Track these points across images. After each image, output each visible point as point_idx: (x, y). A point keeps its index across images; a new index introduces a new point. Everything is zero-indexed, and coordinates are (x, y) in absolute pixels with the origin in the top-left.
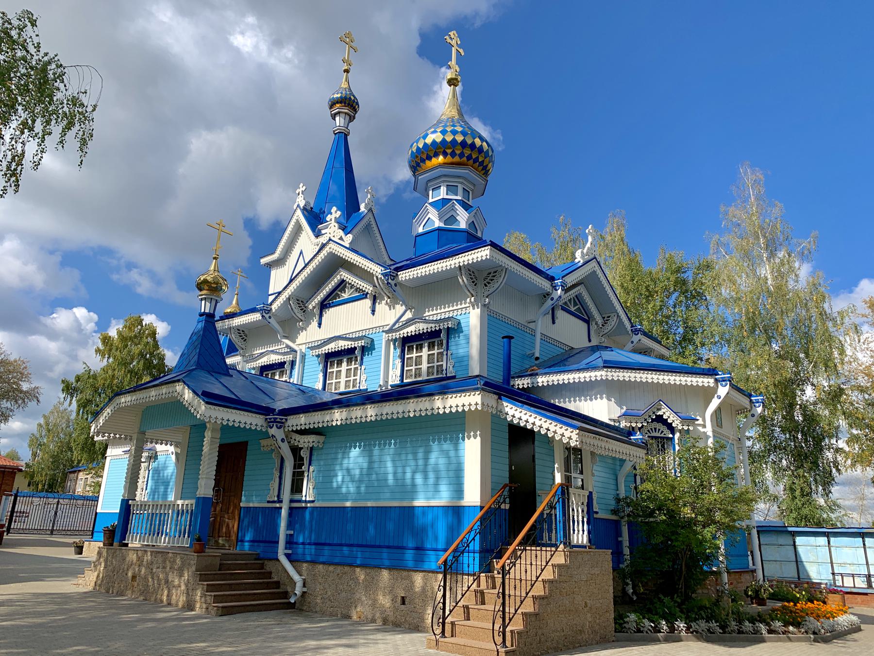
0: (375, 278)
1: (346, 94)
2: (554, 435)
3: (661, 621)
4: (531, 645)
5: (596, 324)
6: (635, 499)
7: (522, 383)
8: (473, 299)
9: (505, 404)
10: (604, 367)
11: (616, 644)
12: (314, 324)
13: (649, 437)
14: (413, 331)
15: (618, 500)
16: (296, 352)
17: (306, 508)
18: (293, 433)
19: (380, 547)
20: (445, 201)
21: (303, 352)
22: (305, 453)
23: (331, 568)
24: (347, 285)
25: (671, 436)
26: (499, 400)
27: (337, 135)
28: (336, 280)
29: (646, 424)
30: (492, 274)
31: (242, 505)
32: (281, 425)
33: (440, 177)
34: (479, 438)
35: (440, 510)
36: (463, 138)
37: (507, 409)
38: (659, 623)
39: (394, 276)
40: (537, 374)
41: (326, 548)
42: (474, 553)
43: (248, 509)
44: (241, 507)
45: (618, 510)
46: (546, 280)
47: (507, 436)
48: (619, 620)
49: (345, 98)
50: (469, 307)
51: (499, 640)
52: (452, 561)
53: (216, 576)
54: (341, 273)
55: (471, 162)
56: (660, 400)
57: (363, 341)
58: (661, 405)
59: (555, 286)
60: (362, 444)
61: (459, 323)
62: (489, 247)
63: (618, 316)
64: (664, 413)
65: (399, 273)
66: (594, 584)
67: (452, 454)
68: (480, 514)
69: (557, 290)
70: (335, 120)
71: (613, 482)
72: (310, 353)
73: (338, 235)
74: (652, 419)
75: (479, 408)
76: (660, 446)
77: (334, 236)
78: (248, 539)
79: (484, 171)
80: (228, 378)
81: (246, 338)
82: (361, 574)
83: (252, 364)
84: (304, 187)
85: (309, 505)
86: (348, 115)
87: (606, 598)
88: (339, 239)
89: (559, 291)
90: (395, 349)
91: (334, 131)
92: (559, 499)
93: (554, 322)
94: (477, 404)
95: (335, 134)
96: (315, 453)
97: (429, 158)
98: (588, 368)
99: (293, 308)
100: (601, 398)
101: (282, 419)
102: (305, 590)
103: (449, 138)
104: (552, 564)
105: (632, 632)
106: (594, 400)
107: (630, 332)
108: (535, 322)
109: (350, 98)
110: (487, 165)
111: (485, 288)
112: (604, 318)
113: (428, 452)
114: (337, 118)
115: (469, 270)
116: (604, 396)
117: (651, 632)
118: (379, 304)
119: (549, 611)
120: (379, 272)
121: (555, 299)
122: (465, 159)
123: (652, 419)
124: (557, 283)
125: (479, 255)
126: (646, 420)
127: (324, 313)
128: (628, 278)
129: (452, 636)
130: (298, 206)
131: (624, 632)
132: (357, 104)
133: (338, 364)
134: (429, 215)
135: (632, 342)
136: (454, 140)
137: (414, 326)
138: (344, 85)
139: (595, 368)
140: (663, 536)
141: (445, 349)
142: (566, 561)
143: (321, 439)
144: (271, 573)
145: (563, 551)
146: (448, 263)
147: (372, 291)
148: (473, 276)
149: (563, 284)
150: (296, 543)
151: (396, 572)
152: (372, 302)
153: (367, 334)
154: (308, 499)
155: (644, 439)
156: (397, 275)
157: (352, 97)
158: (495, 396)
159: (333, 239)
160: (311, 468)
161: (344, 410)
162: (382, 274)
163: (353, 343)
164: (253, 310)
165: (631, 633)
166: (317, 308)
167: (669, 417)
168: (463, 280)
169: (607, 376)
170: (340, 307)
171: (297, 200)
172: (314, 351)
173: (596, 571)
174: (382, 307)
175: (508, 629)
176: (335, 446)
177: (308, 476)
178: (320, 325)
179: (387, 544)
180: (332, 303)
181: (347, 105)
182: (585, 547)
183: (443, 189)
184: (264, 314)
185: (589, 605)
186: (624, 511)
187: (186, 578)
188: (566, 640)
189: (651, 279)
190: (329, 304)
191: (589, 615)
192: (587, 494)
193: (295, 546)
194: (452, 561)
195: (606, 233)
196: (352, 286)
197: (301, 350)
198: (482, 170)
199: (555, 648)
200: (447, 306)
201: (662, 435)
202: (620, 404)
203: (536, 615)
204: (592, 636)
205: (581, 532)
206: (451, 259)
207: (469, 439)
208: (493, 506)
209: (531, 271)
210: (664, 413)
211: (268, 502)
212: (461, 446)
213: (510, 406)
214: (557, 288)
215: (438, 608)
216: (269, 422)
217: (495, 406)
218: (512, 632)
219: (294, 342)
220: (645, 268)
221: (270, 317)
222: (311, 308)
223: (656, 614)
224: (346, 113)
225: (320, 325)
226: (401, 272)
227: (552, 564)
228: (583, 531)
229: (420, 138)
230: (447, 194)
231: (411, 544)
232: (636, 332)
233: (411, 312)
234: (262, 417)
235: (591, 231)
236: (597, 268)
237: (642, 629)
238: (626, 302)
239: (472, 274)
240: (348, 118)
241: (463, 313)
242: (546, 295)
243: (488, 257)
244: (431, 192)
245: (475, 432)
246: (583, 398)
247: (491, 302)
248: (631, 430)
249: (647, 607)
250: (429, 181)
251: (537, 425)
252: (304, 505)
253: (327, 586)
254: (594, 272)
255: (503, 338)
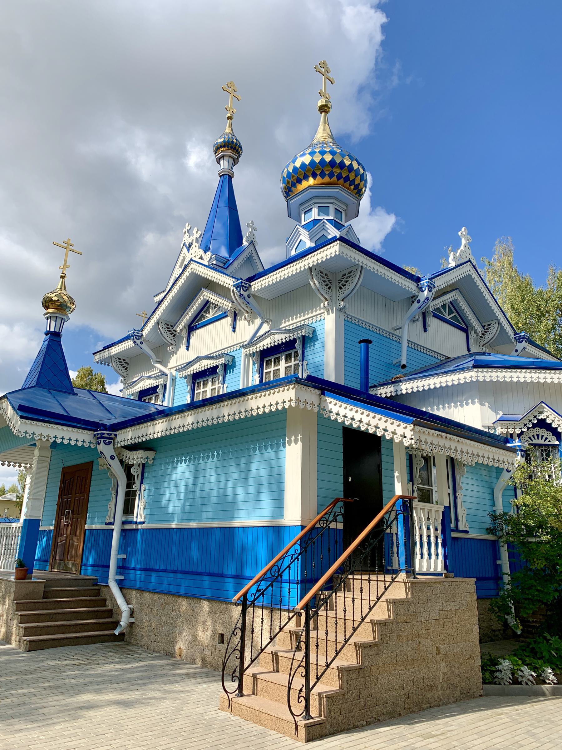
0: (231, 293)
1: (229, 138)
2: (393, 436)
3: (546, 669)
4: (351, 711)
5: (476, 332)
6: (515, 516)
7: (385, 392)
8: (326, 303)
9: (328, 399)
10: (474, 367)
11: (482, 701)
12: (184, 347)
13: (530, 444)
14: (269, 343)
15: (494, 517)
16: (167, 375)
17: (138, 529)
18: (122, 449)
19: (201, 574)
20: (316, 221)
21: (173, 376)
22: (136, 470)
23: (156, 597)
24: (211, 305)
25: (557, 443)
26: (322, 396)
27: (222, 178)
28: (199, 301)
29: (525, 430)
30: (347, 275)
31: (86, 527)
32: (110, 441)
33: (311, 199)
34: (300, 443)
35: (218, 530)
36: (332, 157)
37: (331, 406)
38: (543, 671)
39: (247, 287)
40: (400, 381)
41: (153, 574)
42: (289, 583)
43: (92, 530)
44: (86, 530)
45: (495, 529)
46: (411, 281)
47: (340, 441)
48: (489, 666)
49: (228, 141)
50: (324, 313)
51: (298, 708)
52: (255, 596)
53: (37, 605)
54: (204, 293)
55: (342, 181)
56: (542, 402)
57: (223, 359)
58: (544, 408)
59: (422, 288)
60: (188, 458)
61: (314, 331)
62: (338, 242)
63: (499, 323)
64: (548, 417)
65: (252, 284)
66: (450, 624)
67: (274, 462)
68: (301, 533)
69: (423, 291)
70: (220, 164)
71: (488, 497)
72: (179, 375)
73: (198, 254)
74: (533, 424)
75: (293, 404)
76: (544, 455)
77: (195, 257)
78: (90, 563)
79: (357, 190)
80: (73, 397)
81: (127, 366)
82: (184, 603)
83: (131, 390)
84: (190, 226)
85: (140, 527)
86: (232, 157)
87: (469, 641)
88: (199, 258)
89: (426, 292)
90: (254, 364)
91: (219, 175)
92: (397, 515)
93: (425, 330)
94: (291, 400)
95: (220, 177)
96: (146, 470)
97: (299, 181)
98: (456, 370)
99: (162, 332)
100: (473, 403)
101: (111, 434)
102: (132, 620)
103: (317, 159)
104: (387, 600)
105: (507, 683)
106: (465, 405)
107: (513, 340)
108: (401, 328)
109: (233, 141)
110: (359, 184)
111: (340, 291)
112: (484, 327)
113: (249, 463)
114: (222, 162)
115: (321, 272)
116: (476, 400)
117: (533, 683)
118: (239, 321)
119: (380, 662)
120: (231, 284)
121: (422, 301)
122: (335, 178)
123: (533, 424)
124: (424, 283)
125: (328, 252)
126: (525, 425)
127: (192, 335)
128: (519, 299)
129: (254, 694)
130: (184, 244)
131: (495, 683)
132: (240, 146)
133: (204, 385)
134: (301, 238)
135: (516, 351)
136: (323, 161)
137: (269, 338)
138: (228, 130)
139: (463, 370)
140: (546, 559)
141: (301, 358)
142: (407, 595)
143: (151, 454)
144: (105, 600)
145: (404, 582)
146: (298, 266)
147: (231, 307)
148: (326, 279)
149: (429, 284)
150: (128, 568)
151: (214, 604)
152: (232, 319)
153: (229, 352)
154: (139, 521)
155: (524, 447)
156: (250, 285)
157: (235, 141)
158: (316, 390)
159: (194, 259)
160: (143, 486)
161: (165, 420)
162: (234, 286)
163: (214, 361)
164: (127, 338)
165: (504, 684)
166: (184, 331)
167: (553, 421)
168: (314, 283)
169: (477, 376)
170: (206, 327)
171: (184, 239)
172: (181, 373)
173: (454, 606)
174: (241, 324)
175: (314, 691)
176: (167, 461)
177: (139, 495)
178: (188, 347)
179: (207, 571)
180: (198, 324)
181: (230, 148)
182: (440, 575)
183: (315, 211)
184: (135, 340)
185: (443, 651)
186: (502, 530)
187: (7, 606)
188: (407, 701)
189: (543, 299)
190: (196, 326)
191: (443, 664)
192: (442, 508)
193: (127, 571)
194: (255, 596)
195: (495, 260)
196: (216, 306)
197: (171, 373)
198: (354, 189)
199: (390, 713)
200: (302, 314)
201: (546, 442)
202: (494, 409)
203: (359, 669)
204: (448, 692)
205: (433, 557)
206: (300, 261)
207: (290, 445)
208: (318, 525)
209: (389, 269)
210: (548, 417)
211: (106, 524)
212: (281, 454)
213: (334, 401)
214: (424, 289)
215: (232, 657)
216: (98, 438)
217: (316, 403)
218: (320, 695)
219: (166, 366)
220: (535, 289)
221: (141, 343)
222: (178, 331)
223: (541, 658)
224: (229, 156)
225: (188, 347)
226: (254, 283)
227: (387, 600)
228: (437, 555)
229: (290, 163)
230: (319, 215)
231: (231, 571)
232: (519, 339)
233: (268, 325)
234: (89, 432)
235: (464, 233)
236: (472, 272)
237: (520, 679)
238: (517, 323)
239: (325, 277)
240: (231, 160)
241: (318, 320)
242: (413, 299)
243: (337, 253)
244: (303, 216)
245: (296, 437)
246: (452, 404)
247: (347, 305)
248: (509, 437)
249: (531, 646)
250: (302, 204)
251: (364, 422)
252: (134, 526)
253: (152, 617)
254: (470, 276)
255: (360, 342)
